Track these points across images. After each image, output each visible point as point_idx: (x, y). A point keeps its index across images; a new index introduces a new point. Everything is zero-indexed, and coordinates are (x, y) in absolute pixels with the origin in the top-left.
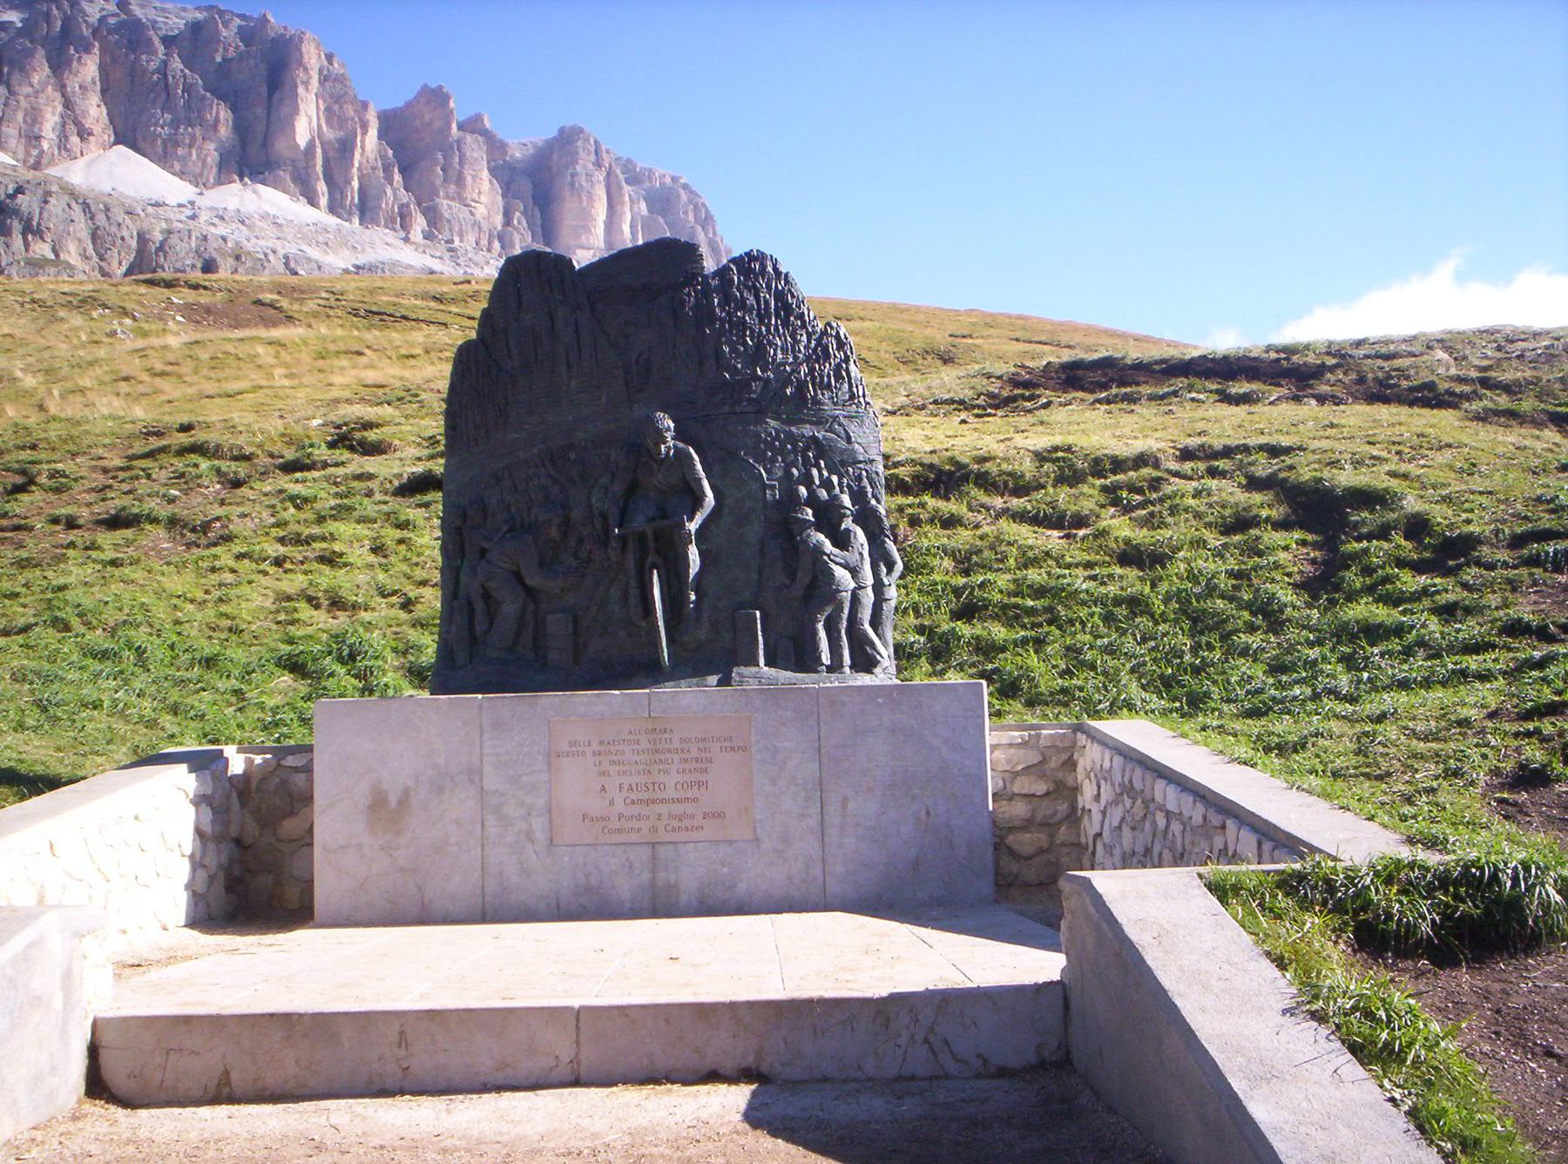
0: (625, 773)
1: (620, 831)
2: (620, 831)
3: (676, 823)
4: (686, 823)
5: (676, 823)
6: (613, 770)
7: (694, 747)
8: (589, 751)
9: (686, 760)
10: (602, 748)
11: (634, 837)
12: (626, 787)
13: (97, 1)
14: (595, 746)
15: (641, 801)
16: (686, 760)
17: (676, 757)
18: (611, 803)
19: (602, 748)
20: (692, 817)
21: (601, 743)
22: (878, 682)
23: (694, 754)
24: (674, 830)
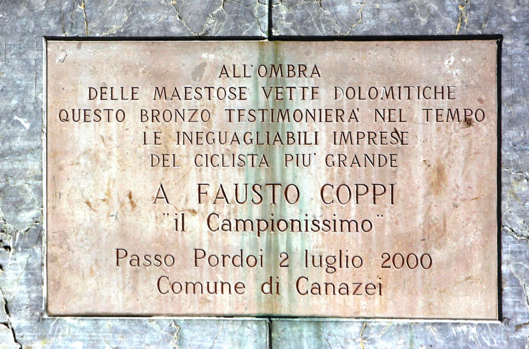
0: (211, 160)
1: (191, 287)
2: (191, 287)
3: (319, 276)
4: (345, 275)
5: (319, 276)
6: (184, 151)
7: (365, 108)
8: (133, 110)
9: (346, 138)
10: (161, 104)
11: (225, 302)
12: (212, 191)
13: (521, 0)
14: (146, 99)
15: (370, 159)
16: (346, 138)
17: (321, 127)
18: (180, 225)
19: (161, 104)
20: (357, 262)
21: (161, 92)
22: (365, 146)
23: (366, 123)
24: (316, 289)
